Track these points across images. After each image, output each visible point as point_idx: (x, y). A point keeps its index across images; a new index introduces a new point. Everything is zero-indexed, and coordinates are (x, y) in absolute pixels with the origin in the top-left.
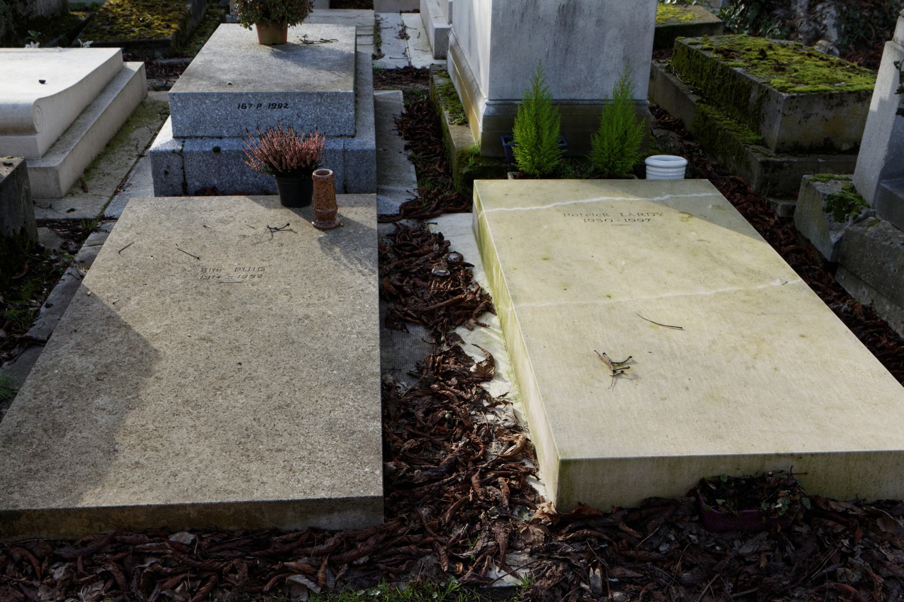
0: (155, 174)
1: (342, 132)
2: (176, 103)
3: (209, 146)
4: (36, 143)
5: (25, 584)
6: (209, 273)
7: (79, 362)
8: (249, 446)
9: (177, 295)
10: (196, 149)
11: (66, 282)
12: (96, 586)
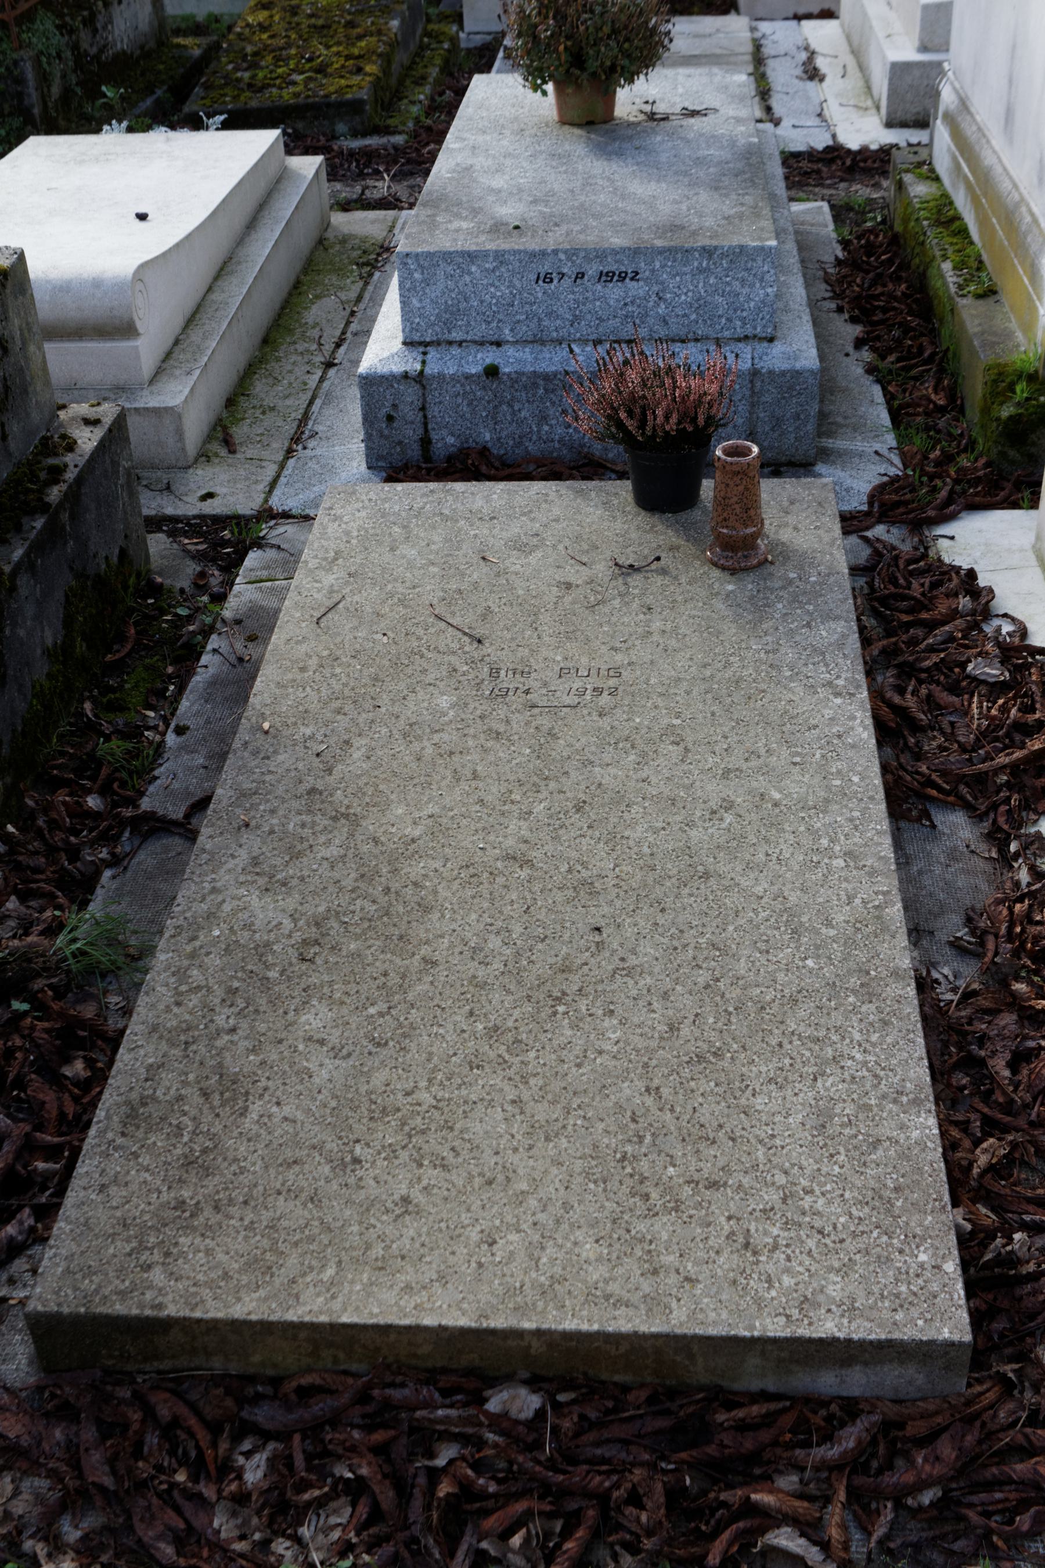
0: (368, 420)
1: (749, 331)
2: (411, 274)
3: (475, 362)
4: (138, 357)
5: (184, 1491)
6: (506, 681)
7: (265, 910)
8: (644, 1165)
9: (445, 736)
10: (451, 370)
11: (211, 670)
12: (336, 1512)
